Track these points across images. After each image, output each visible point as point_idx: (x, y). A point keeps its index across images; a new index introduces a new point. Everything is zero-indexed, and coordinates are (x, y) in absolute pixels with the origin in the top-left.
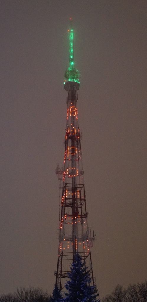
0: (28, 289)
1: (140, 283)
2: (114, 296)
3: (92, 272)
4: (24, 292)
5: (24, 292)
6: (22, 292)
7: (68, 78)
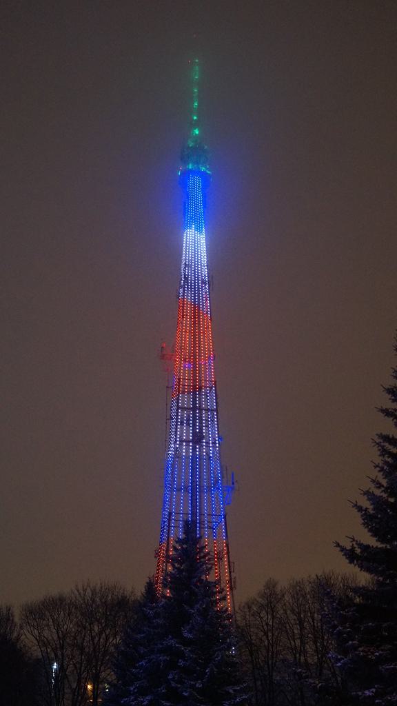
0: (97, 584)
1: (313, 576)
2: (261, 599)
3: (228, 553)
4: (89, 591)
5: (89, 591)
6: (85, 590)
7: (186, 163)
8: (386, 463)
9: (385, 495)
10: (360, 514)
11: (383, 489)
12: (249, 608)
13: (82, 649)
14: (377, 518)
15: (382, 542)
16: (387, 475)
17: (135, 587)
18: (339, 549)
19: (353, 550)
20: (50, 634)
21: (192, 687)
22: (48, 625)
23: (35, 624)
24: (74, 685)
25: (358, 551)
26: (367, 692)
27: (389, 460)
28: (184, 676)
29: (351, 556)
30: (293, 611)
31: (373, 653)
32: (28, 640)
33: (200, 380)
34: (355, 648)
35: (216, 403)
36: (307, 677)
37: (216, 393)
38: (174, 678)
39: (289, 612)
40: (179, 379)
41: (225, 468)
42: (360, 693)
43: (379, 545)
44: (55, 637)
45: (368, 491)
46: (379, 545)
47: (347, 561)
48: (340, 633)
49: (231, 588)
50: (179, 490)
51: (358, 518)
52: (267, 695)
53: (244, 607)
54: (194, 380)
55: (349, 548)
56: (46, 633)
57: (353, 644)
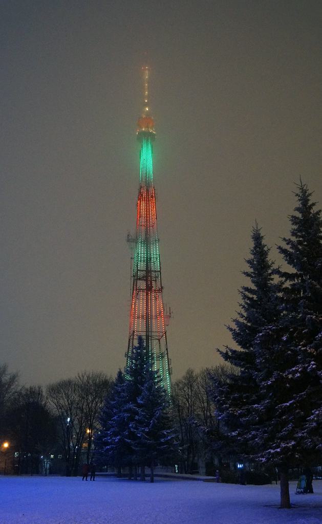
3: (167, 354)
4: (85, 377)
5: (85, 377)
6: (83, 376)
8: (246, 303)
9: (245, 322)
10: (231, 333)
11: (244, 318)
12: (178, 385)
13: (82, 410)
14: (241, 334)
15: (244, 348)
16: (247, 310)
17: (112, 376)
18: (219, 352)
19: (227, 353)
20: (64, 402)
21: (143, 431)
22: (62, 397)
23: (55, 396)
24: (78, 431)
25: (230, 354)
26: (233, 433)
27: (248, 302)
28: (138, 425)
29: (226, 356)
30: (203, 387)
31: (237, 411)
32: (51, 405)
33: (150, 254)
34: (227, 409)
35: (160, 267)
36: (200, 425)
37: (159, 261)
38: (133, 426)
39: (200, 387)
40: (138, 253)
41: (165, 305)
42: (229, 434)
43: (242, 350)
44: (67, 404)
45: (236, 320)
46: (242, 350)
47: (224, 359)
48: (219, 401)
49: (170, 374)
50: (138, 318)
51: (230, 335)
52: (188, 435)
53: (175, 385)
54: (147, 254)
55: (225, 352)
56: (61, 402)
57: (226, 407)
